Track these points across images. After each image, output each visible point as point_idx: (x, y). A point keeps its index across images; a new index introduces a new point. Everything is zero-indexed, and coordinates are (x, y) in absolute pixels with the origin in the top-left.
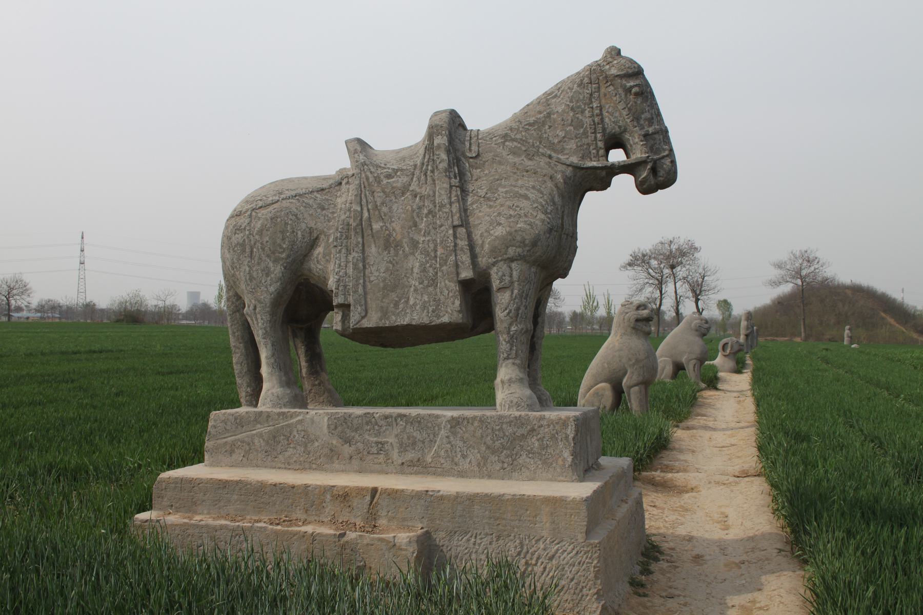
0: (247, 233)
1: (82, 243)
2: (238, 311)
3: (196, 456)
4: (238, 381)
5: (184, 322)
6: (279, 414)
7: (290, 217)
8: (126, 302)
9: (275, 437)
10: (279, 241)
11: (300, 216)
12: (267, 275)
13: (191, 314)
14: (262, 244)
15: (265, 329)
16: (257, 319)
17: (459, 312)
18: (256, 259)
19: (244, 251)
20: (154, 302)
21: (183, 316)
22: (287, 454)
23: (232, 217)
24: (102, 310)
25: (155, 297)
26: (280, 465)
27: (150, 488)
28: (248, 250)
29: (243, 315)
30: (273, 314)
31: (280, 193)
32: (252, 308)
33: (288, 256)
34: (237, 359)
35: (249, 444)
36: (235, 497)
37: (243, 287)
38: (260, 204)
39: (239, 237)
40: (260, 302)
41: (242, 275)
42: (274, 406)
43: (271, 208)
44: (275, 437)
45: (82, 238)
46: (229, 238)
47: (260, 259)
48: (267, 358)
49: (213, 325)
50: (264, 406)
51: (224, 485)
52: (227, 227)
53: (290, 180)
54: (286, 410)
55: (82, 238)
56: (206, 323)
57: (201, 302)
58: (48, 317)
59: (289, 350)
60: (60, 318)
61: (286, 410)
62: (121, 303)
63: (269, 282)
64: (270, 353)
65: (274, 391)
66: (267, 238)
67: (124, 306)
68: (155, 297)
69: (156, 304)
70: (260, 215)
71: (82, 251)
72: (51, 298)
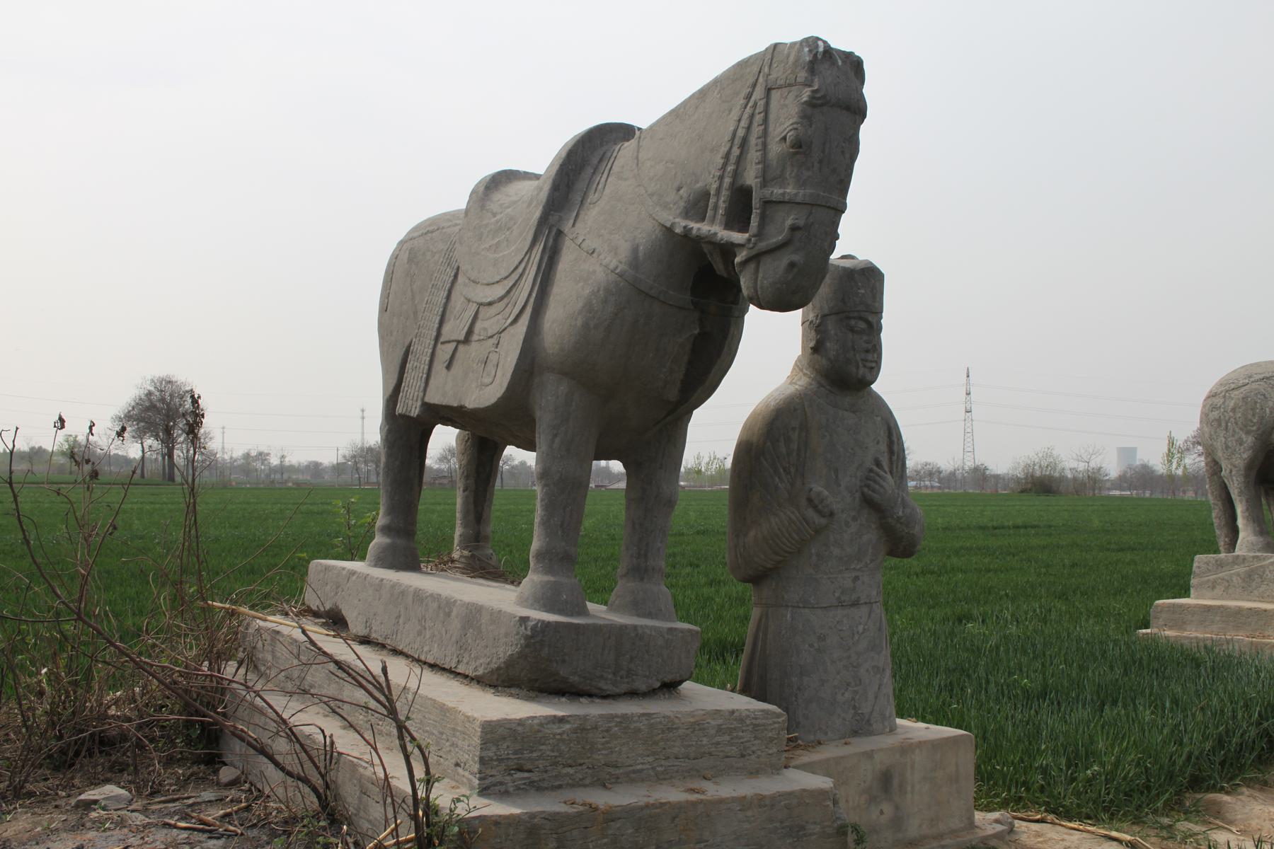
0: (1222, 410)
1: (968, 383)
2: (1216, 474)
3: (1185, 592)
4: (1218, 532)
5: (1117, 493)
6: (1254, 557)
7: (1259, 396)
8: (1034, 465)
9: (1250, 576)
10: (1250, 417)
11: (1268, 396)
12: (1241, 445)
13: (1122, 481)
14: (1235, 419)
15: (1240, 488)
16: (1233, 481)
17: (231, 458)
18: (1231, 431)
19: (1220, 425)
20: (1073, 464)
21: (1112, 484)
22: (1261, 589)
23: (1208, 397)
24: (997, 477)
25: (1075, 456)
26: (1254, 598)
27: (1148, 613)
28: (1223, 424)
29: (1221, 477)
30: (1246, 476)
31: (1250, 377)
32: (1228, 471)
33: (1258, 429)
34: (1216, 516)
35: (1228, 581)
36: (1218, 618)
37: (1220, 454)
38: (1233, 386)
39: (1215, 414)
40: (1235, 466)
41: (1219, 444)
42: (1249, 551)
43: (1242, 390)
44: (1250, 576)
45: (968, 376)
46: (1207, 415)
47: (1234, 431)
48: (1242, 512)
49: (1159, 496)
50: (1240, 550)
51: (1209, 609)
52: (1204, 406)
53: (1258, 365)
54: (1259, 554)
55: (968, 376)
56: (1147, 494)
57: (1138, 463)
58: (926, 487)
59: (1261, 505)
60: (939, 488)
61: (1259, 554)
62: (1027, 466)
63: (1242, 450)
64: (1245, 508)
65: (1249, 539)
66: (1240, 415)
67: (1031, 470)
68: (1075, 456)
69: (1076, 466)
70: (1232, 395)
71: (968, 394)
72: (929, 460)
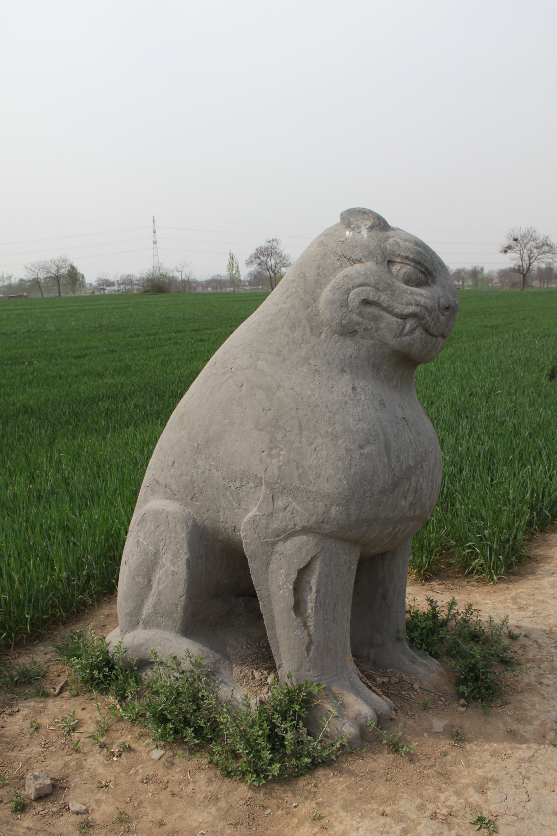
1: (154, 226)
45: (154, 221)
55: (154, 221)
71: (154, 232)
